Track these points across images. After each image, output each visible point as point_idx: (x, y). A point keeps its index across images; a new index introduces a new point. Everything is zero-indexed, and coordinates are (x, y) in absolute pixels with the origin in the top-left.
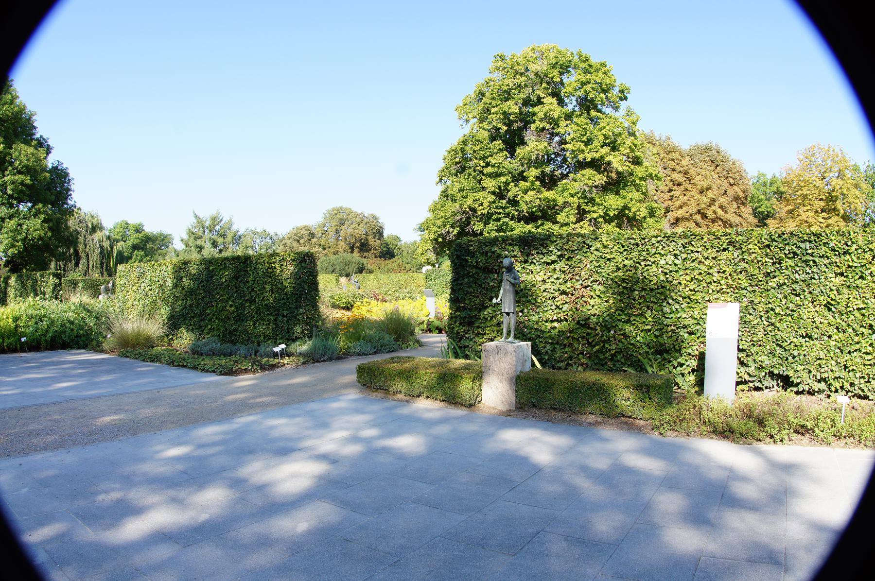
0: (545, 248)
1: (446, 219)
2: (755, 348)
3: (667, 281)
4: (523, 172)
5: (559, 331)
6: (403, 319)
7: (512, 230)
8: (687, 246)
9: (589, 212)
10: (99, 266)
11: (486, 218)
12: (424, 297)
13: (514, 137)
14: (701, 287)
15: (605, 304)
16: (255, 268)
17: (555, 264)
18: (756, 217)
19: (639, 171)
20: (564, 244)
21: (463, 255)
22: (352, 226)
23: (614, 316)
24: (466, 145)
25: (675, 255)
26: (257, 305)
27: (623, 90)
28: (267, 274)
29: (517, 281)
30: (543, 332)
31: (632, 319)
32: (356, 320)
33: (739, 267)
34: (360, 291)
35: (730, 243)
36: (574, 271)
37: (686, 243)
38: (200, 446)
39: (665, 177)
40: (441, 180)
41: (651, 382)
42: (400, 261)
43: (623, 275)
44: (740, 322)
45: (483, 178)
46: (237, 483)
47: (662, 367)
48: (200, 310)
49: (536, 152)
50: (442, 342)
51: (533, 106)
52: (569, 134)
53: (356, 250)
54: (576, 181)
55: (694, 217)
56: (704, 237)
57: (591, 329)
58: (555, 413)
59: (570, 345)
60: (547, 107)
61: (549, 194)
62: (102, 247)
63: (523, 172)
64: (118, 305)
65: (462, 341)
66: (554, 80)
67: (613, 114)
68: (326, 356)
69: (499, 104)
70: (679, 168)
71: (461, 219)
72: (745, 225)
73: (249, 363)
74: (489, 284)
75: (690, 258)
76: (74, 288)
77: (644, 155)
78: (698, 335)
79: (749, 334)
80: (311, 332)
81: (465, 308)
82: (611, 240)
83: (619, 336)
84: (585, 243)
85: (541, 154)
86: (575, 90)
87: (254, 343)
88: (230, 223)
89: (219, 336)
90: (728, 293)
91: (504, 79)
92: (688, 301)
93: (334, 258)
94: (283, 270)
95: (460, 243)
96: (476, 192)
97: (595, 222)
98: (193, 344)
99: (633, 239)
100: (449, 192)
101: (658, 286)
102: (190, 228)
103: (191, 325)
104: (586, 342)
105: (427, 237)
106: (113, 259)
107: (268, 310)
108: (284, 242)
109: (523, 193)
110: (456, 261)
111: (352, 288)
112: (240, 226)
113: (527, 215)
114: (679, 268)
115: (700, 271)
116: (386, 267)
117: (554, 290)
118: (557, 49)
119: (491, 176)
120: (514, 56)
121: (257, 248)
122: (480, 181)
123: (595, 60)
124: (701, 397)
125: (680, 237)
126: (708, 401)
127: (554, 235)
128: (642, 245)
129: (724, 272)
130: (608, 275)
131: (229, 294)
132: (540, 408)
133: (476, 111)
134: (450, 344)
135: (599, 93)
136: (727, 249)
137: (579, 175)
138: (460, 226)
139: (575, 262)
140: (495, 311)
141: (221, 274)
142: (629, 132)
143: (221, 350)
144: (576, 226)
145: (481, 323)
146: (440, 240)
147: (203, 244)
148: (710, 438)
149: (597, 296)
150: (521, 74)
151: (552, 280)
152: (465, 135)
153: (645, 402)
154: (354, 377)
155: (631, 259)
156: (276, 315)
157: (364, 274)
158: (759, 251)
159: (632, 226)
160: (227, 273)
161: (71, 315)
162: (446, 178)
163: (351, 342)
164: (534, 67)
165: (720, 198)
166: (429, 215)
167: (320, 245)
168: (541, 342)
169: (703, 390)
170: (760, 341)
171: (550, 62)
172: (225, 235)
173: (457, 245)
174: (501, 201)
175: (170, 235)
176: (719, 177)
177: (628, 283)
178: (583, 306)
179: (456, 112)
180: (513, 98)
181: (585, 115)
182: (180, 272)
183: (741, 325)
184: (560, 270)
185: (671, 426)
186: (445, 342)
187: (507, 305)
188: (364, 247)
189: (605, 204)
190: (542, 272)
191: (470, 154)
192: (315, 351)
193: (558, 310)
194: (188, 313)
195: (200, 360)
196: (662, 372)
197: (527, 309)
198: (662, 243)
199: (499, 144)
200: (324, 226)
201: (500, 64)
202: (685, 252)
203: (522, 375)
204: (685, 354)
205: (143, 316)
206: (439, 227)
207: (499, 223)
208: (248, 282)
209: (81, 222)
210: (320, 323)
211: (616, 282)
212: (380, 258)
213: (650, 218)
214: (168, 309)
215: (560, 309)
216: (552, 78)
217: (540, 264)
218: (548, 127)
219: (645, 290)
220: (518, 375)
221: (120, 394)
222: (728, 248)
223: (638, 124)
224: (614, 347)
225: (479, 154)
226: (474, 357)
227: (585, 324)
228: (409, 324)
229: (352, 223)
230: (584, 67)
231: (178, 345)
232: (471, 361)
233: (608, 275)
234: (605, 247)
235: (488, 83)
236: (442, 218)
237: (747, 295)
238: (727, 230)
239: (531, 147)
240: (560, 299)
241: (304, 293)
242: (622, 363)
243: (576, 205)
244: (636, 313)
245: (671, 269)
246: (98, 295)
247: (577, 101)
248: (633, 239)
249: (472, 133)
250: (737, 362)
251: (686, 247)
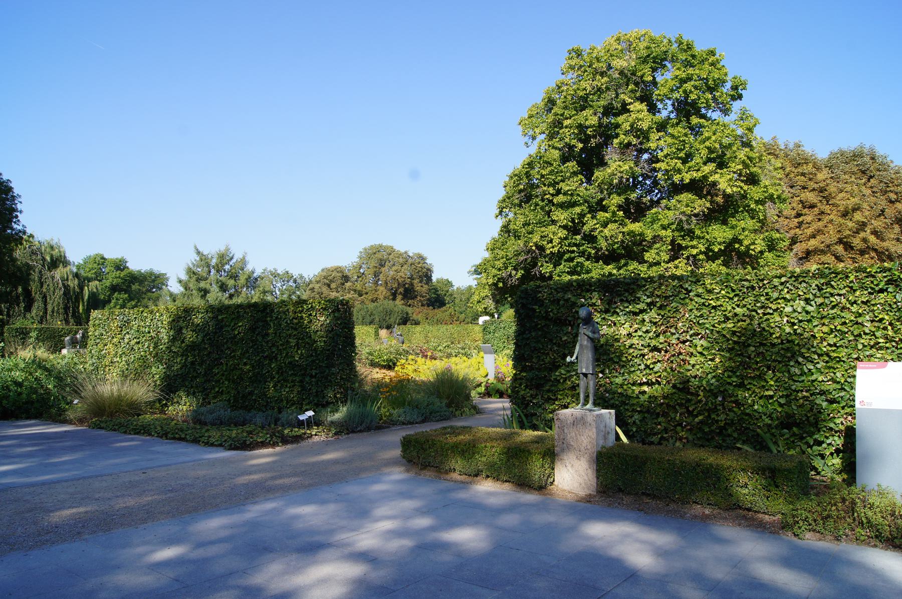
0: (631, 294)
1: (507, 260)
4: (602, 200)
5: (650, 397)
6: (457, 380)
7: (588, 272)
8: (824, 287)
9: (686, 248)
11: (556, 259)
12: (482, 354)
15: (710, 363)
17: (644, 314)
19: (755, 192)
20: (655, 289)
22: (394, 268)
23: (722, 378)
25: (807, 301)
26: (278, 363)
29: (596, 336)
30: (629, 397)
32: (401, 381)
34: (405, 347)
35: (889, 282)
36: (668, 322)
37: (823, 284)
38: (200, 545)
41: (777, 465)
43: (734, 327)
47: (790, 446)
50: (504, 409)
51: (617, 115)
52: (662, 150)
53: (399, 297)
54: (669, 209)
55: (832, 248)
56: (850, 275)
57: (692, 394)
59: (665, 414)
60: (634, 116)
61: (636, 227)
62: (66, 287)
63: (602, 200)
64: (90, 362)
65: (529, 408)
66: (645, 79)
67: (721, 119)
69: (574, 115)
70: (812, 185)
71: (526, 259)
73: (267, 434)
74: (561, 338)
75: (829, 303)
76: (24, 338)
77: (763, 171)
78: (844, 404)
80: (346, 396)
81: (531, 368)
83: (730, 404)
84: (682, 288)
86: (672, 91)
87: (273, 409)
88: (243, 261)
89: (229, 400)
90: (887, 348)
91: (580, 81)
94: (311, 321)
95: (526, 289)
96: (544, 226)
97: (694, 260)
99: (747, 280)
100: (511, 227)
101: (782, 341)
102: (191, 266)
103: (192, 387)
105: (484, 281)
106: (83, 303)
108: (311, 286)
111: (394, 342)
112: (257, 265)
114: (812, 316)
115: (843, 320)
116: (436, 318)
117: (642, 345)
118: (650, 36)
119: (563, 206)
120: (592, 49)
122: (548, 213)
123: (700, 48)
124: (852, 488)
125: (814, 276)
126: (864, 494)
127: (643, 278)
129: (881, 320)
130: (714, 326)
131: (242, 350)
133: (545, 125)
134: (514, 412)
135: (704, 92)
136: (886, 290)
137: (673, 201)
138: (524, 269)
139: (669, 311)
141: (232, 324)
142: (742, 142)
144: (669, 265)
145: (552, 386)
146: (501, 285)
147: (208, 286)
148: (872, 546)
149: (699, 353)
150: (603, 74)
151: (640, 333)
152: (530, 156)
153: (769, 491)
154: (397, 452)
155: (745, 306)
156: (303, 375)
157: (408, 326)
161: (18, 375)
162: (507, 210)
164: (618, 63)
165: (873, 222)
166: (487, 255)
167: (355, 291)
168: (627, 410)
169: (855, 478)
173: (522, 292)
174: (574, 237)
176: (873, 192)
178: (680, 365)
179: (520, 126)
180: (591, 106)
182: (179, 321)
184: (651, 322)
185: (810, 525)
187: (584, 365)
188: (408, 293)
189: (708, 237)
190: (627, 323)
193: (648, 371)
195: (204, 430)
196: (792, 452)
197: (609, 369)
198: (788, 285)
199: (572, 165)
200: (361, 267)
202: (822, 295)
205: (126, 377)
206: (499, 270)
207: (572, 264)
208: (267, 335)
209: (33, 253)
210: (357, 385)
212: (428, 306)
213: (769, 252)
216: (642, 76)
218: (634, 141)
219: (765, 345)
221: (88, 477)
222: (887, 288)
223: (755, 130)
224: (723, 417)
225: (548, 179)
226: (544, 427)
227: (684, 388)
228: (464, 386)
229: (394, 265)
230: (684, 58)
231: (174, 413)
233: (714, 326)
234: (710, 292)
235: (559, 87)
236: (503, 258)
238: (886, 264)
240: (650, 357)
241: (337, 349)
242: (735, 438)
243: (669, 239)
244: (752, 375)
245: (800, 318)
247: (673, 105)
248: (747, 280)
249: (540, 153)
251: (823, 289)
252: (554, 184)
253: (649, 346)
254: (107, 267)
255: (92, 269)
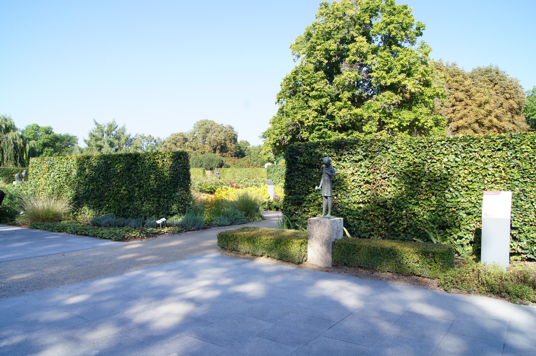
2: (526, 227)
3: (449, 174)
4: (339, 94)
6: (251, 200)
7: (330, 137)
8: (466, 147)
9: (387, 123)
10: (13, 158)
11: (311, 129)
12: (266, 185)
13: (332, 68)
14: (478, 179)
15: (399, 191)
16: (143, 163)
17: (361, 162)
18: (528, 124)
20: (368, 147)
21: (295, 155)
22: (215, 134)
23: (406, 200)
24: (297, 75)
25: (456, 155)
26: (144, 190)
27: (419, 27)
28: (152, 167)
29: (333, 174)
31: (420, 202)
33: (512, 163)
34: (221, 181)
35: (504, 145)
36: (375, 166)
37: (465, 146)
39: (450, 95)
40: (279, 100)
41: (436, 250)
42: (249, 159)
43: (414, 170)
44: (513, 206)
45: (309, 99)
46: (123, 322)
47: (444, 239)
48: (100, 193)
49: (349, 79)
50: (278, 217)
51: (348, 43)
52: (374, 65)
53: (218, 151)
54: (378, 100)
56: (481, 140)
57: (388, 209)
58: (361, 271)
59: (372, 221)
60: (358, 44)
61: (358, 111)
62: (15, 144)
63: (339, 94)
64: (30, 189)
65: (293, 217)
66: (365, 22)
67: (410, 48)
68: (196, 227)
70: (461, 88)
71: (293, 129)
72: (518, 130)
73: (138, 232)
74: (313, 176)
75: (469, 156)
78: (475, 215)
79: (521, 216)
80: (185, 209)
81: (295, 193)
82: (404, 144)
83: (410, 215)
84: (384, 146)
85: (352, 81)
86: (381, 29)
87: (141, 217)
88: (124, 129)
89: (115, 212)
90: (501, 183)
91: (327, 23)
92: (466, 189)
93: (201, 157)
94: (164, 164)
95: (292, 146)
96: (304, 109)
97: (391, 131)
98: (93, 218)
99: (422, 142)
100: (285, 110)
101: (441, 178)
102: (92, 132)
103: (92, 204)
104: (384, 218)
105: (268, 142)
107: (153, 193)
108: (165, 144)
109: (338, 110)
110: (289, 159)
111: (214, 178)
112: (132, 132)
113: (340, 126)
114: (459, 164)
115: (477, 167)
117: (360, 180)
119: (315, 97)
121: (145, 148)
122: (307, 102)
124: (479, 263)
125: (461, 141)
126: (485, 267)
127: (361, 141)
128: (429, 147)
129: (498, 167)
130: (402, 169)
132: (350, 267)
133: (305, 48)
135: (400, 31)
136: (502, 149)
137: (380, 96)
138: (292, 135)
139: (376, 160)
140: (317, 195)
141: (116, 166)
142: (422, 62)
143: (116, 223)
144: (377, 134)
145: (306, 204)
146: (278, 144)
147: (102, 144)
148: (489, 297)
149: (393, 185)
150: (340, 18)
151: (358, 173)
152: (296, 67)
153: (431, 265)
154: (215, 241)
155: (420, 158)
156: (159, 197)
157: (223, 168)
158: (531, 150)
159: (421, 134)
160: (121, 166)
162: (282, 100)
163: (213, 217)
164: (350, 12)
165: (496, 110)
166: (270, 126)
167: (191, 147)
169: (480, 258)
170: (531, 221)
171: (363, 7)
172: (120, 138)
173: (290, 148)
174: (322, 116)
175: (75, 137)
176: (497, 93)
177: (417, 176)
180: (333, 38)
181: (388, 50)
183: (513, 209)
184: (365, 166)
185: (454, 285)
186: (281, 217)
188: (223, 149)
189: (400, 117)
191: (300, 81)
192: (187, 223)
193: (363, 195)
194: (90, 195)
195: (99, 230)
196: (445, 243)
198: (445, 146)
199: (321, 73)
200: (195, 133)
201: (324, 10)
202: (465, 152)
203: (337, 241)
204: (464, 230)
206: (277, 135)
207: (320, 132)
210: (192, 202)
211: (408, 175)
212: (235, 157)
213: (436, 127)
214: (73, 192)
215: (365, 194)
216: (364, 21)
217: (350, 162)
218: (358, 59)
219: (431, 180)
220: (333, 242)
221: (30, 258)
222: (502, 148)
223: (430, 55)
224: (406, 222)
225: (306, 81)
227: (384, 205)
228: (255, 204)
230: (389, 10)
231: (82, 219)
232: (299, 231)
234: (400, 149)
235: (314, 26)
236: (279, 128)
237: (519, 185)
239: (345, 76)
240: (364, 187)
241: (179, 181)
242: (412, 235)
243: (377, 118)
244: (423, 198)
245: (452, 165)
246: (13, 181)
247: (382, 38)
248: (422, 142)
249: (302, 65)
250: (509, 237)
251: (465, 148)
252: (310, 84)
253: (364, 180)
254: (40, 132)
255: (31, 133)
